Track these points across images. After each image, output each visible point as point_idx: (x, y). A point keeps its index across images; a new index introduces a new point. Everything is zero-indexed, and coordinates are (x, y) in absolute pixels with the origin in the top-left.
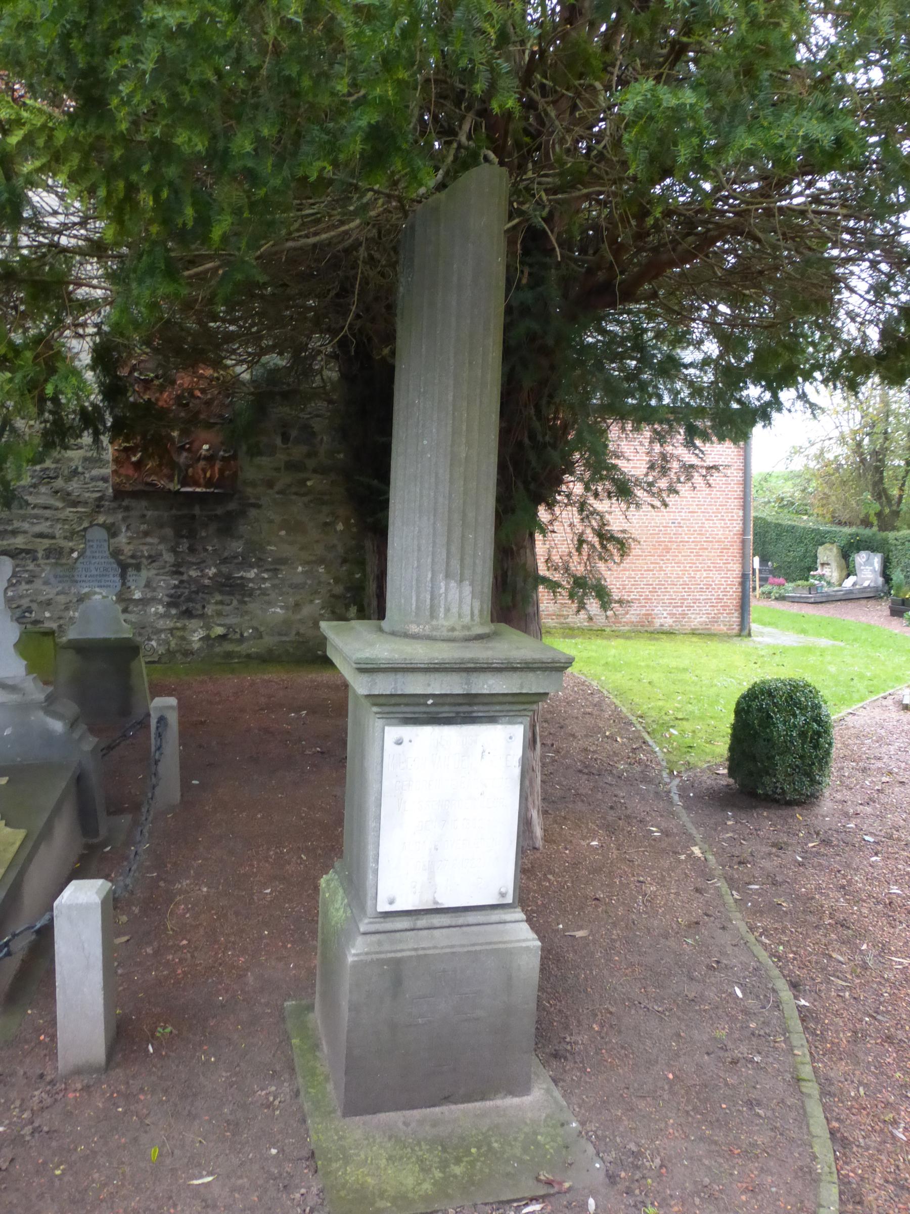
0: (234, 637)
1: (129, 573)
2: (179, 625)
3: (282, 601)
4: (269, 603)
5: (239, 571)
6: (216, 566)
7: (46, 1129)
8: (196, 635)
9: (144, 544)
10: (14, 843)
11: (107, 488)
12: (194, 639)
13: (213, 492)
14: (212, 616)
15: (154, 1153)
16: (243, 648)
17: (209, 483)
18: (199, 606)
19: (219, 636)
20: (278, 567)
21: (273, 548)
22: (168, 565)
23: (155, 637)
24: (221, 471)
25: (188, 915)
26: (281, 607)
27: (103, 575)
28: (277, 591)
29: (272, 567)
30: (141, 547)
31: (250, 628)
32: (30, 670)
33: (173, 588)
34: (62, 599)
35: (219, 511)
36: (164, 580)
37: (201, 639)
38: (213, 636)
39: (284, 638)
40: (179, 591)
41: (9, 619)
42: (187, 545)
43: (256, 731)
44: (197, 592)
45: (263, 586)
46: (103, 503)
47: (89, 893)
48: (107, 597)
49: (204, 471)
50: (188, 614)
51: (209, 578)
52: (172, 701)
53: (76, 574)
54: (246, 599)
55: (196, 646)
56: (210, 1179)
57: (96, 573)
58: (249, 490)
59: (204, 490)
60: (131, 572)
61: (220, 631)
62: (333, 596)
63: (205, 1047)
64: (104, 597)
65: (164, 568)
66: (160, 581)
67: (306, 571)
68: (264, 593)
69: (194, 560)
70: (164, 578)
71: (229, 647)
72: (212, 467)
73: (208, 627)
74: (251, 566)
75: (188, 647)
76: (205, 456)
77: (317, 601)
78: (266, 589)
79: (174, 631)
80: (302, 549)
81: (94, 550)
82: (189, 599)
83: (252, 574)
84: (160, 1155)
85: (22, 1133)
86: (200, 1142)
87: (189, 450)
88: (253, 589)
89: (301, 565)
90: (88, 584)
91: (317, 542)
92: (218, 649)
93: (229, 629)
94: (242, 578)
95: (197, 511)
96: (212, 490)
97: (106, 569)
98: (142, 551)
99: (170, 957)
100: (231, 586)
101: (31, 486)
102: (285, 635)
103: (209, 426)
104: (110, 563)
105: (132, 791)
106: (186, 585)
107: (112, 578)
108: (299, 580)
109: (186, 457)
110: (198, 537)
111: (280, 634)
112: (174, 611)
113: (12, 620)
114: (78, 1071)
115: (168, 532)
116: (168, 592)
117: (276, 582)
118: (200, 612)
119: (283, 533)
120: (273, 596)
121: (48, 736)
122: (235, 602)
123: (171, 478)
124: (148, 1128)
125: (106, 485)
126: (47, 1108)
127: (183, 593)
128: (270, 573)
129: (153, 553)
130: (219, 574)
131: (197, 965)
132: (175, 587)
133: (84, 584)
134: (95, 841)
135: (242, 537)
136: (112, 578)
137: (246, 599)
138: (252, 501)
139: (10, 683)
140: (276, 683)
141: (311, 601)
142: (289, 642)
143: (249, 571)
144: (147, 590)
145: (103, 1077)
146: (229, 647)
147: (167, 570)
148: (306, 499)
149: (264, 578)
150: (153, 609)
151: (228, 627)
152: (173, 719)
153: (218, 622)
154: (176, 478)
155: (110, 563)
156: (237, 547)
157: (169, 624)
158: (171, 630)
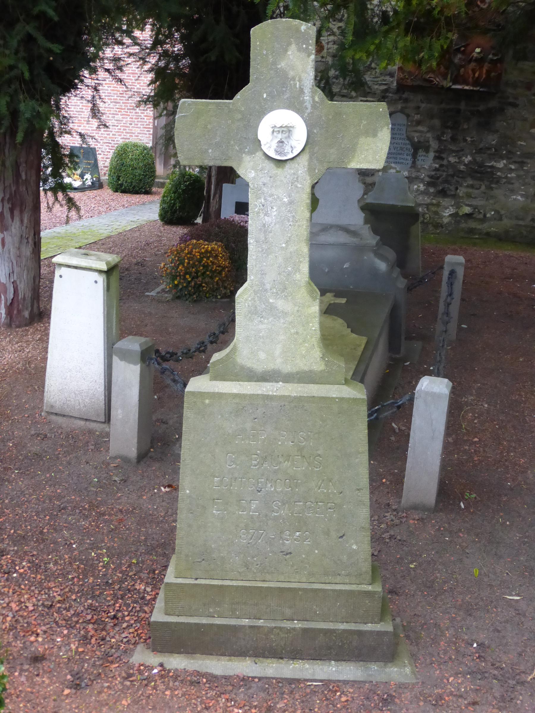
0: (478, 217)
2: (434, 201)
3: (522, 190)
4: (512, 191)
5: (491, 160)
6: (472, 155)
7: (399, 538)
8: (447, 211)
9: (416, 131)
10: (360, 346)
11: (392, 82)
12: (445, 214)
13: (478, 91)
14: (463, 197)
15: (476, 572)
16: (485, 227)
17: (476, 83)
18: (452, 188)
19: (466, 214)
20: (525, 160)
21: (522, 143)
24: (488, 72)
25: (476, 421)
26: (522, 196)
27: (399, 154)
28: (520, 181)
29: (520, 160)
31: (493, 210)
32: (366, 222)
35: (482, 108)
38: (461, 214)
39: (521, 223)
40: (439, 173)
41: (357, 180)
42: (450, 135)
43: (507, 295)
44: (453, 176)
45: (509, 175)
46: (387, 94)
47: (441, 386)
48: (400, 172)
49: (474, 71)
50: (443, 193)
51: (465, 165)
52: (461, 259)
54: (493, 186)
55: (446, 221)
56: (518, 598)
59: (471, 88)
60: (421, 152)
61: (467, 210)
63: (502, 514)
64: (397, 172)
68: (509, 182)
69: (454, 148)
71: (473, 224)
72: (481, 68)
73: (458, 206)
74: (502, 158)
75: (439, 221)
76: (476, 57)
78: (512, 178)
79: (430, 206)
82: (446, 181)
83: (501, 164)
84: (480, 574)
85: (383, 536)
86: (507, 574)
87: (463, 53)
88: (500, 177)
92: (463, 225)
93: (475, 209)
94: (492, 167)
95: (463, 106)
96: (478, 88)
97: (402, 149)
99: (467, 447)
100: (481, 173)
101: (334, 78)
102: (522, 219)
103: (485, 32)
104: (406, 144)
105: (417, 325)
106: (444, 168)
107: (405, 156)
109: (460, 59)
111: (517, 218)
112: (432, 190)
113: (359, 181)
114: (415, 507)
115: (437, 122)
117: (522, 173)
118: (453, 193)
120: (517, 185)
121: (374, 272)
122: (483, 188)
123: (445, 77)
124: (468, 555)
125: (391, 79)
126: (397, 525)
127: (441, 176)
128: (517, 165)
130: (474, 161)
131: (488, 457)
132: (436, 170)
134: (398, 356)
135: (497, 131)
136: (405, 156)
137: (493, 186)
138: (511, 100)
139: (352, 228)
140: (517, 258)
142: (526, 226)
143: (499, 162)
144: (413, 170)
145: (432, 515)
146: (473, 224)
149: (511, 169)
150: (416, 187)
151: (475, 207)
152: (460, 272)
153: (467, 203)
154: (449, 77)
155: (406, 144)
156: (492, 140)
157: (427, 200)
158: (428, 205)
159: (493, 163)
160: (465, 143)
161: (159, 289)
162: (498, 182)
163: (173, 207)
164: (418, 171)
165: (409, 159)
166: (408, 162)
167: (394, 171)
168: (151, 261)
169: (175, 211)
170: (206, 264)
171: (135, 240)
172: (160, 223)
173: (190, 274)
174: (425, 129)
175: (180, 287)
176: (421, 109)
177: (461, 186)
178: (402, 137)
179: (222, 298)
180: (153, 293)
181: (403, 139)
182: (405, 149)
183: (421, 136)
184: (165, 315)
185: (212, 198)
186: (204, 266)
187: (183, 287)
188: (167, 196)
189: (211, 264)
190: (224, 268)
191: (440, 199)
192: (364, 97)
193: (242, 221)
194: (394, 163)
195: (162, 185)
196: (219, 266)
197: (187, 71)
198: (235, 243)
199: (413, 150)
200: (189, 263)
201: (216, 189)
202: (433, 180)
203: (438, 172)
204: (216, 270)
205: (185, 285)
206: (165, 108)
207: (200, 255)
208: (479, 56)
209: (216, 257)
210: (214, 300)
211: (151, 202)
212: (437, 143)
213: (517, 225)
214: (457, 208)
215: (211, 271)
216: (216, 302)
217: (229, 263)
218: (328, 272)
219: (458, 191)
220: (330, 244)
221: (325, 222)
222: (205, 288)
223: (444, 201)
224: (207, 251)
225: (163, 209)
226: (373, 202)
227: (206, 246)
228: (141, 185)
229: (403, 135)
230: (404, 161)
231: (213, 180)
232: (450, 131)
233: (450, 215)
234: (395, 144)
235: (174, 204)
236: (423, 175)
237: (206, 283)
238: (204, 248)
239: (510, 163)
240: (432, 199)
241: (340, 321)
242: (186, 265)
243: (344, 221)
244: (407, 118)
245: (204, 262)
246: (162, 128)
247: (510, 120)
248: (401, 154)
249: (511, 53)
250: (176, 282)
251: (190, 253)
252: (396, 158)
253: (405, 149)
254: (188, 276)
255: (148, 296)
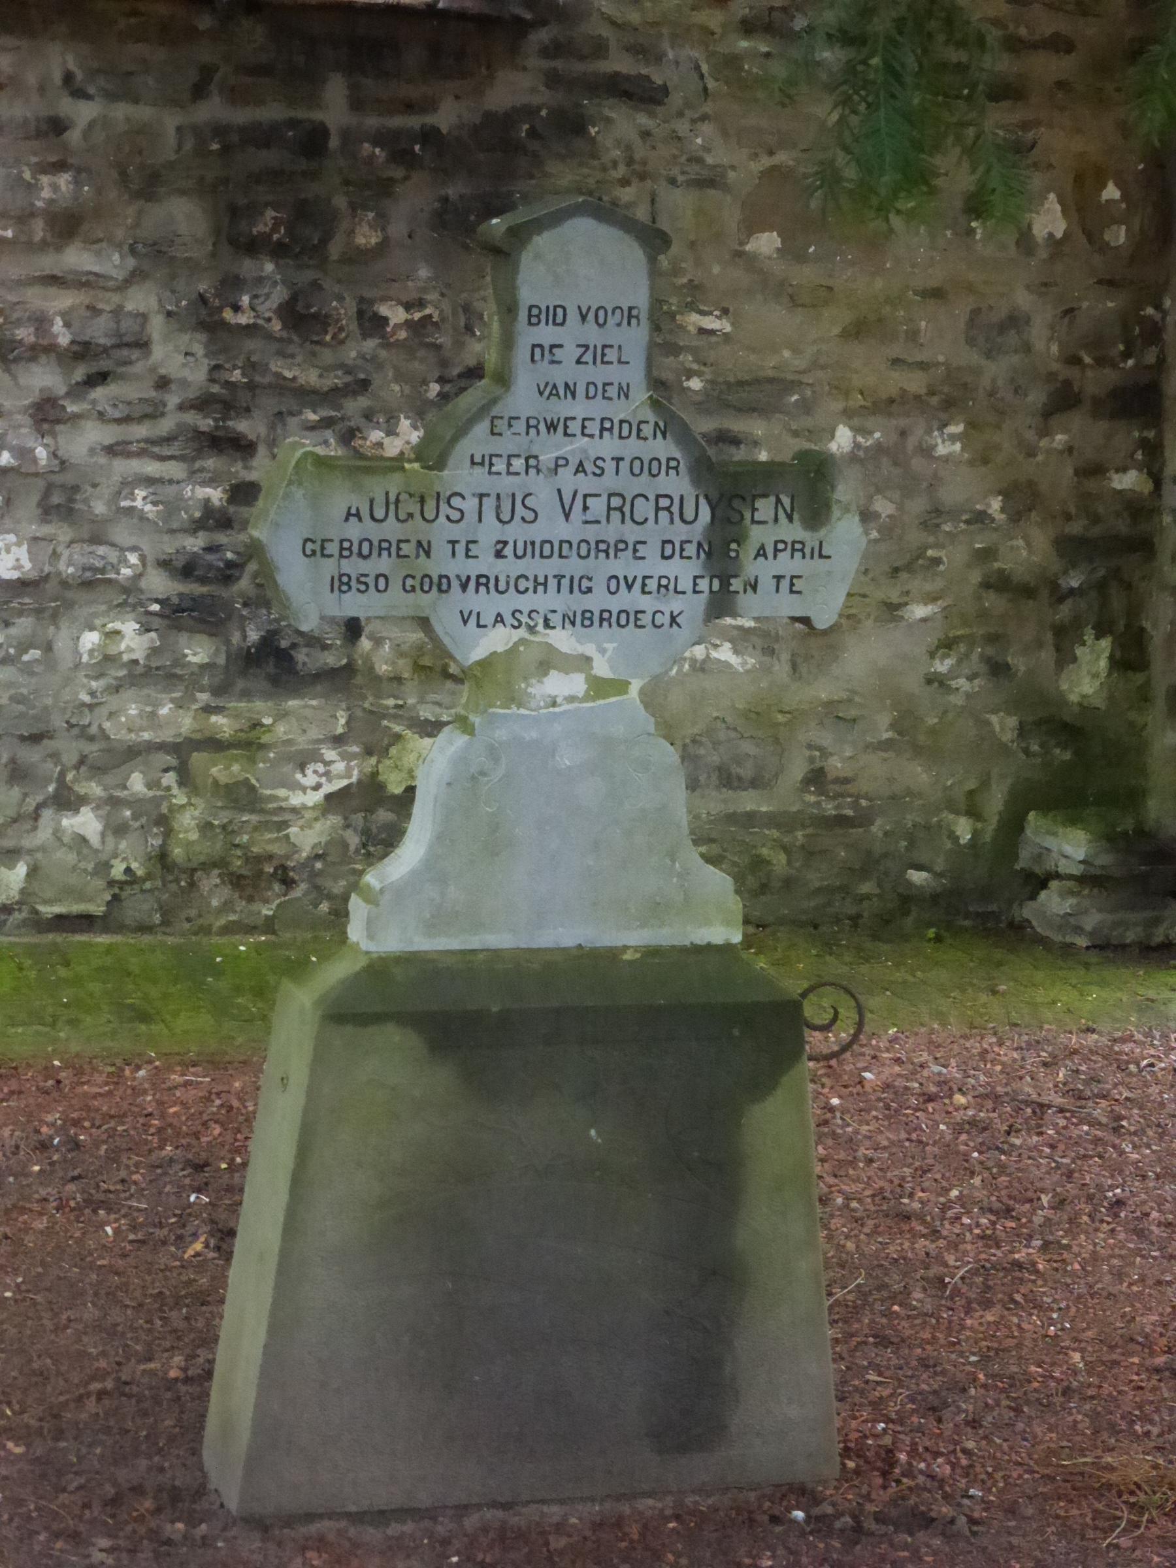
1: (758, 535)
2: (222, 724)
8: (310, 779)
9: (53, 280)
12: (296, 799)
21: (710, 323)
22: (173, 400)
23: (94, 789)
27: (602, 548)
30: (38, 299)
33: (198, 526)
36: (149, 481)
37: (334, 801)
39: (749, 802)
42: (279, 295)
53: (441, 532)
57: (561, 530)
62: (1000, 583)
64: (600, 688)
65: (154, 413)
66: (128, 485)
67: (880, 449)
69: (311, 377)
70: (152, 468)
75: (265, 843)
77: (920, 611)
79: (197, 759)
80: (857, 331)
81: (559, 375)
89: (848, 415)
90: (507, 603)
91: (936, 294)
98: (41, 322)
102: (755, 783)
104: (651, 467)
107: (654, 566)
110: (335, 250)
111: (728, 780)
116: (170, 545)
118: (331, 659)
119: (766, 243)
129: (99, 331)
133: (485, 603)
138: (620, 64)
141: (892, 610)
142: (772, 820)
144: (63, 532)
147: (166, 426)
150: (90, 639)
155: (651, 467)
160: (370, 344)
164: (96, 539)
165: (685, 584)
166: (676, 604)
167: (576, 684)
174: (114, 264)
176: (74, 136)
178: (619, 410)
181: (634, 429)
182: (644, 509)
183: (93, 310)
191: (259, 705)
194: (570, 620)
199: (705, 514)
202: (198, 589)
203: (222, 538)
212: (199, 349)
213: (731, 818)
214: (369, 752)
219: (365, 644)
223: (281, 716)
226: (423, 943)
229: (623, 391)
230: (647, 603)
232: (269, 267)
233: (329, 797)
234: (566, 474)
236: (133, 558)
240: (208, 710)
244: (652, 260)
247: (625, 182)
248: (620, 546)
252: (581, 585)
253: (644, 509)
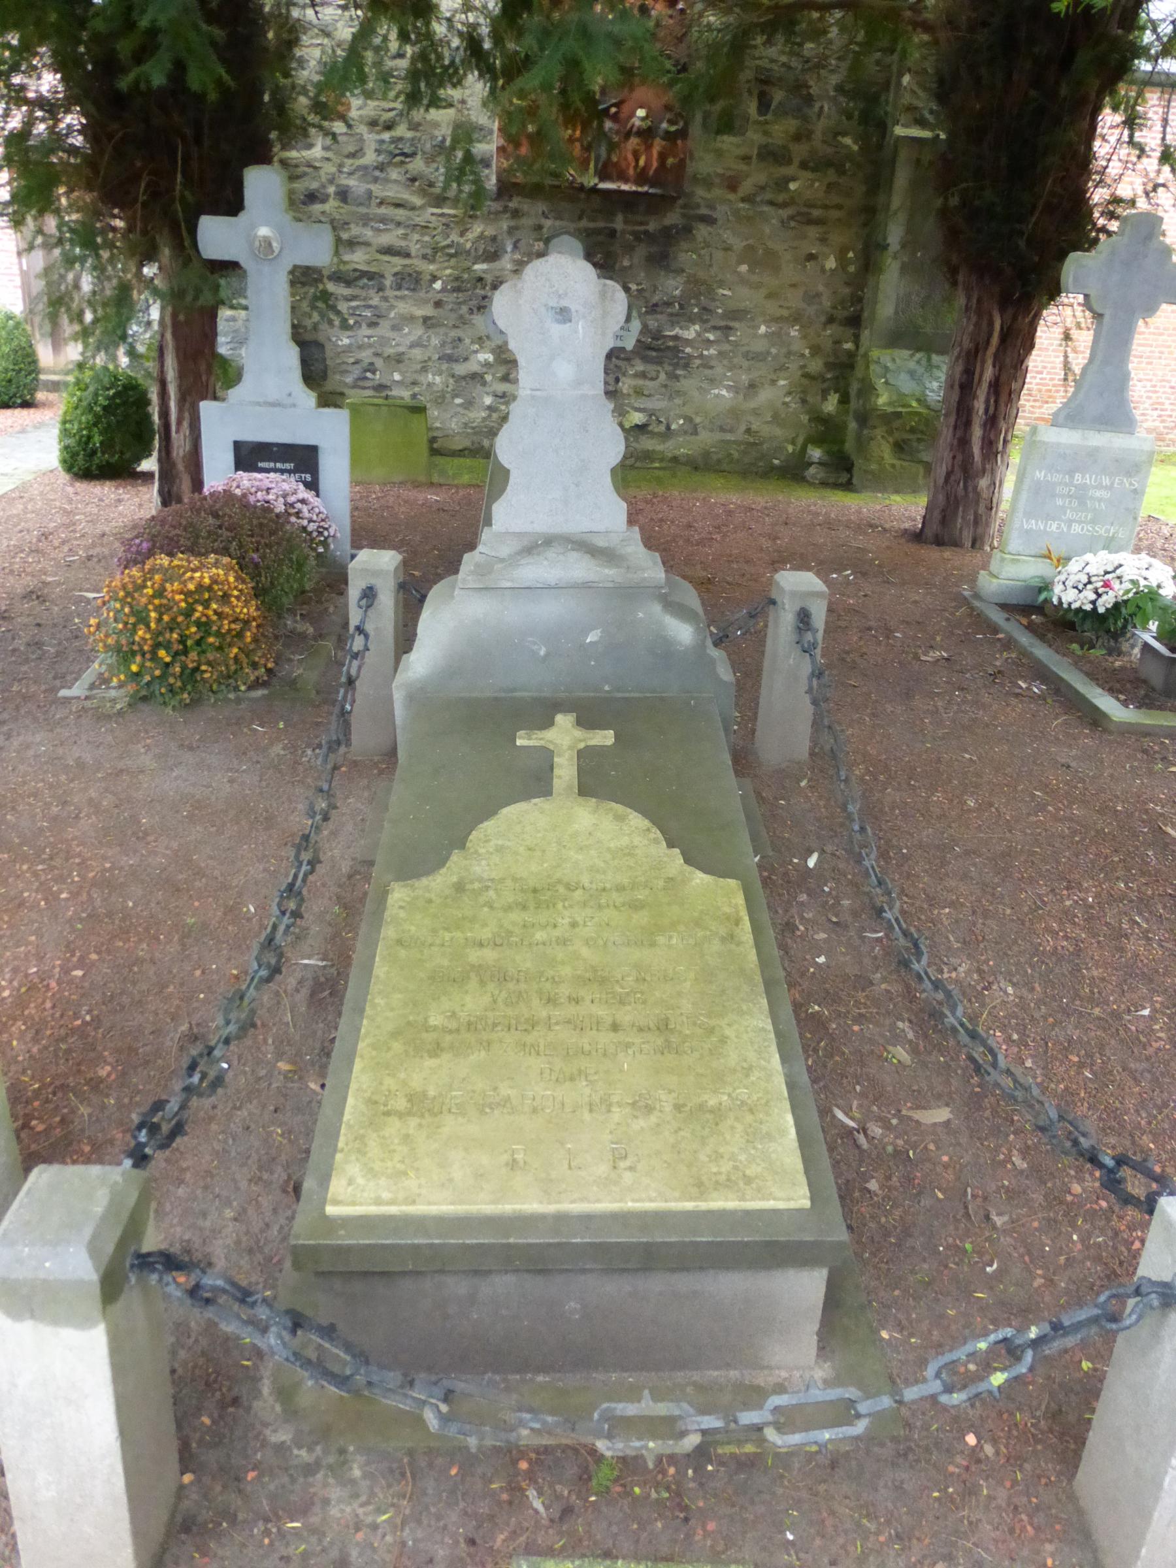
4: (712, 381)
5: (673, 325)
13: (646, 193)
16: (668, 448)
17: (641, 178)
19: (637, 426)
20: (732, 324)
24: (662, 157)
26: (729, 388)
28: (725, 362)
29: (723, 323)
31: (680, 417)
34: (417, 353)
35: (652, 226)
54: (679, 372)
58: (700, 192)
72: (649, 147)
74: (692, 320)
78: (710, 357)
83: (690, 333)
88: (690, 356)
94: (676, 338)
95: (619, 223)
96: (646, 189)
101: (376, 168)
102: (731, 431)
108: (759, 346)
111: (722, 429)
117: (726, 347)
119: (744, 268)
120: (719, 370)
121: (664, 650)
128: (719, 333)
137: (679, 372)
138: (704, 211)
139: (601, 542)
142: (734, 442)
148: (785, 213)
149: (708, 340)
151: (651, 413)
154: (592, 165)
156: (674, 286)
159: (677, 331)
161: (88, 677)
162: (686, 366)
163: (87, 443)
168: (59, 584)
169: (94, 453)
170: (204, 619)
171: (15, 526)
172: (64, 477)
173: (167, 646)
175: (147, 678)
177: (624, 375)
179: (250, 688)
180: (77, 690)
184: (121, 765)
185: (173, 428)
186: (198, 624)
187: (154, 678)
188: (70, 421)
189: (215, 618)
190: (246, 622)
192: (437, 207)
193: (259, 489)
195: (55, 387)
196: (236, 620)
197: (78, 141)
198: (257, 550)
200: (159, 620)
201: (180, 410)
204: (230, 630)
205: (157, 673)
206: (40, 231)
207: (185, 601)
208: (644, 125)
209: (226, 597)
210: (232, 696)
211: (39, 426)
215: (218, 634)
216: (238, 701)
217: (258, 609)
218: (547, 655)
220: (550, 588)
221: (528, 528)
222: (207, 675)
224: (200, 587)
225: (66, 448)
227: (198, 575)
228: (13, 390)
231: (172, 390)
235: (89, 438)
237: (209, 663)
238: (192, 578)
239: (706, 331)
241: (636, 821)
242: (153, 625)
243: (578, 523)
245: (197, 615)
246: (37, 276)
249: (699, 117)
250: (134, 668)
251: (160, 593)
254: (162, 653)
255: (67, 700)
